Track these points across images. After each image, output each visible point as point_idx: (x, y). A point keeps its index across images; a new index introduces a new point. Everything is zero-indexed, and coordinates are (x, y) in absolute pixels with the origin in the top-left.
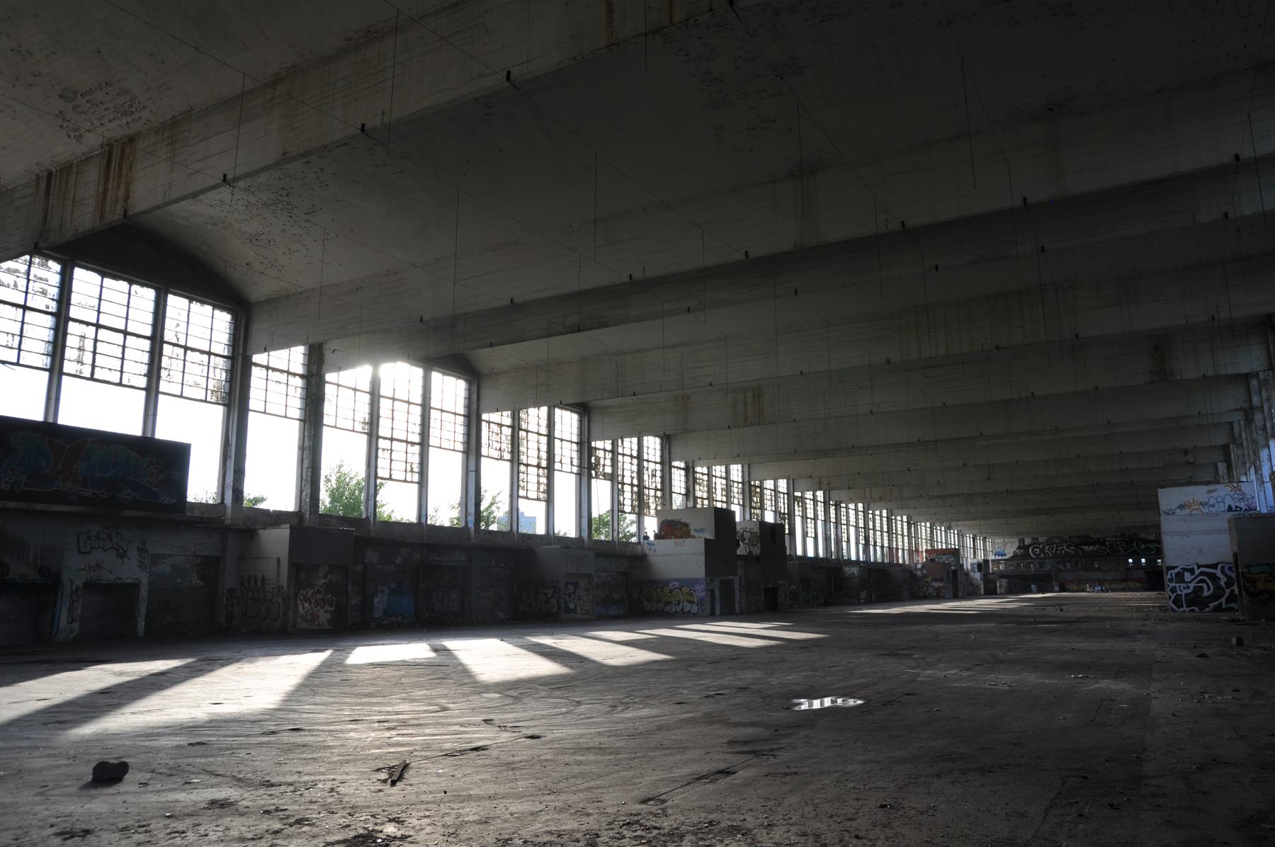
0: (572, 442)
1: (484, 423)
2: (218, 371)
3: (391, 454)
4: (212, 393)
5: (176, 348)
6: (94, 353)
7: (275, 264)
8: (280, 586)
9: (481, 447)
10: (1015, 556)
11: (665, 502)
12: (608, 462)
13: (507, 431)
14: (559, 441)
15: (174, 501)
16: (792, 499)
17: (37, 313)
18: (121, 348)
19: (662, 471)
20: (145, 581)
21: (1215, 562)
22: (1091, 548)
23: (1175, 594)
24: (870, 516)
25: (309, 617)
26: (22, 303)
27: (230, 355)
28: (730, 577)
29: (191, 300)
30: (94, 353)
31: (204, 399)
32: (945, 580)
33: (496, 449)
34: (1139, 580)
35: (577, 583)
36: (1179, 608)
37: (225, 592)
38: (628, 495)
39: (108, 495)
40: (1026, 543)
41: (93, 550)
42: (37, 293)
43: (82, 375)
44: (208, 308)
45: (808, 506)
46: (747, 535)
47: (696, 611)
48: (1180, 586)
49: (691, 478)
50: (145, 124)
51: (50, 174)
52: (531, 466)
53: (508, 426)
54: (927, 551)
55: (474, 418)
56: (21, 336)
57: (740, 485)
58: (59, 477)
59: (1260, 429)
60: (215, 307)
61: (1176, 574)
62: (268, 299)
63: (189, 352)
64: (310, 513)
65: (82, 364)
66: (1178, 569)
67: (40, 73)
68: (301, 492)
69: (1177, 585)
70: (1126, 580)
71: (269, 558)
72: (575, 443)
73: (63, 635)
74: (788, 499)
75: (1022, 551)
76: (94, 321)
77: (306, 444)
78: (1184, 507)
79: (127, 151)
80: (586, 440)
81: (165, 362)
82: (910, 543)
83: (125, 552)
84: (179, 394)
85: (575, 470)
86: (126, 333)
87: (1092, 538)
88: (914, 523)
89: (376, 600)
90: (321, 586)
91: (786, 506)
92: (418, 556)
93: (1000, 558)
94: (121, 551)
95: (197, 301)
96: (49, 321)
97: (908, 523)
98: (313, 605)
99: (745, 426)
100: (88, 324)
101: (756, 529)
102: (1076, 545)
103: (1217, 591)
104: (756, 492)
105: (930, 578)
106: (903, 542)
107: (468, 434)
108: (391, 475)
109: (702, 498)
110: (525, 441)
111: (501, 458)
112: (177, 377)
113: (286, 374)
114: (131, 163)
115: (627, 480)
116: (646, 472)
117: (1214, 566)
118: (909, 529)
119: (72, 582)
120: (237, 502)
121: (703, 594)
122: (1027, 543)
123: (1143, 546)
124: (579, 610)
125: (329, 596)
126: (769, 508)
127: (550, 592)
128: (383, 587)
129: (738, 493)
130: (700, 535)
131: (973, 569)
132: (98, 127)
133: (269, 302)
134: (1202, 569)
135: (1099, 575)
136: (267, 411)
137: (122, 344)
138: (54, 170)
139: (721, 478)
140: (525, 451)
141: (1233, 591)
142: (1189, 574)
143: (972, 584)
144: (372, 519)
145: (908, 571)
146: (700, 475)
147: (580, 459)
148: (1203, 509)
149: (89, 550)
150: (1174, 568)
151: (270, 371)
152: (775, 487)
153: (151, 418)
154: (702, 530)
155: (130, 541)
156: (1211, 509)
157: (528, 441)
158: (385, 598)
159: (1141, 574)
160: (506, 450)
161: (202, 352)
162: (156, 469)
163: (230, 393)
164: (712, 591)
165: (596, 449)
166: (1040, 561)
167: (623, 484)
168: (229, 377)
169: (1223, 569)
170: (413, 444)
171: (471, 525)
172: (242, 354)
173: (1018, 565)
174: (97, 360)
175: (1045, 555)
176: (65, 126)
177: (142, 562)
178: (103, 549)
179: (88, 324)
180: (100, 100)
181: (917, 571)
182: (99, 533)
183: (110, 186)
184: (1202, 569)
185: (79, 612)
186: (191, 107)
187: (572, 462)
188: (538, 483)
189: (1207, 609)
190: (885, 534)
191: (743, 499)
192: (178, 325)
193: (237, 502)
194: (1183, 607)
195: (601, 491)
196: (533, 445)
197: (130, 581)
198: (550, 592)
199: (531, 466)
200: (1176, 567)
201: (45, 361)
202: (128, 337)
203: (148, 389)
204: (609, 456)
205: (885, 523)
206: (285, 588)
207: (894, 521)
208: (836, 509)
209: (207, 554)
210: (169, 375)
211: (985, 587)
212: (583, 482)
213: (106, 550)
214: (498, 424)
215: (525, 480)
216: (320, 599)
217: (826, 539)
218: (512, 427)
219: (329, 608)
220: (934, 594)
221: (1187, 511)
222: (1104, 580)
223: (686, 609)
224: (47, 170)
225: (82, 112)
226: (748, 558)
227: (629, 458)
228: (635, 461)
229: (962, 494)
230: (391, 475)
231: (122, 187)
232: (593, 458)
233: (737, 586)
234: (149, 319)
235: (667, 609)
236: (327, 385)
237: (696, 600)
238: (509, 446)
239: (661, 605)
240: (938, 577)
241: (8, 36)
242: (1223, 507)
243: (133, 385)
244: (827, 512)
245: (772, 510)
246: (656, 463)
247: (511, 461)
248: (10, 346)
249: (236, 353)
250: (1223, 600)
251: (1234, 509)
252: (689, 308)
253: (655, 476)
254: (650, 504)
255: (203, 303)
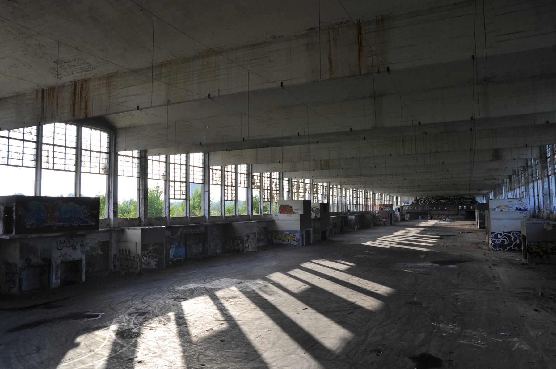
0: (244, 174)
1: (210, 170)
2: (104, 160)
3: (174, 188)
4: (102, 170)
5: (86, 151)
6: (53, 157)
7: (130, 114)
8: (137, 254)
9: (210, 180)
10: (413, 204)
11: (281, 196)
12: (259, 181)
13: (219, 172)
14: (240, 174)
15: (94, 224)
16: (329, 188)
17: (29, 142)
18: (64, 154)
19: (279, 182)
20: (84, 258)
21: (510, 231)
22: (444, 201)
23: (494, 243)
24: (358, 192)
25: (146, 263)
26: (22, 138)
27: (108, 152)
28: (309, 229)
29: (91, 129)
30: (53, 157)
31: (99, 173)
32: (387, 218)
33: (215, 181)
34: (463, 215)
35: (249, 236)
36: (495, 249)
37: (113, 256)
38: (266, 194)
39: (68, 225)
40: (418, 199)
41: (63, 248)
42: (28, 133)
43: (49, 168)
44: (99, 131)
45: (335, 191)
46: (314, 209)
47: (296, 244)
48: (496, 240)
49: (290, 184)
50: (94, 75)
51: (43, 91)
52: (229, 186)
53: (220, 170)
54: (379, 205)
55: (207, 168)
56: (23, 153)
57: (309, 185)
58: (49, 220)
59: (530, 175)
60: (101, 131)
61: (495, 235)
62: (125, 127)
63: (92, 152)
64: (144, 218)
65: (49, 163)
66: (496, 233)
67: (47, 53)
68: (140, 209)
69: (495, 240)
70: (458, 215)
71: (132, 242)
72: (246, 174)
73: (54, 285)
74: (327, 189)
75: (416, 202)
76: (52, 143)
77: (141, 188)
78: (499, 207)
79: (84, 86)
80: (250, 173)
81: (83, 158)
82: (373, 202)
83: (75, 247)
84: (89, 172)
85: (246, 186)
86: (65, 147)
87: (445, 197)
88: (374, 193)
89: (171, 251)
90: (151, 250)
91: (326, 191)
92: (186, 231)
93: (407, 204)
94: (74, 247)
95: (94, 129)
96: (34, 145)
97: (372, 193)
98: (148, 258)
99: (321, 170)
100: (50, 145)
101: (318, 207)
102: (438, 200)
103: (510, 242)
104: (315, 187)
105: (381, 217)
106: (370, 202)
107: (204, 176)
108: (174, 197)
109: (294, 192)
110: (227, 176)
111: (217, 185)
112: (87, 164)
113: (131, 158)
114: (87, 92)
115: (266, 188)
116: (273, 183)
117: (510, 233)
118: (373, 196)
119: (56, 263)
120: (115, 217)
121: (299, 237)
122: (418, 198)
123: (465, 201)
124: (250, 247)
125: (155, 254)
126: (320, 193)
127: (239, 241)
128: (173, 245)
129: (308, 188)
130: (297, 211)
131: (396, 210)
132: (70, 74)
133: (125, 129)
134: (505, 234)
135: (447, 213)
136: (125, 175)
137: (64, 152)
138: (45, 89)
139: (302, 182)
140: (227, 180)
141: (516, 243)
142: (500, 235)
143: (396, 217)
144: (168, 217)
145: (373, 215)
146: (294, 182)
147: (248, 181)
148: (506, 209)
149: (61, 248)
150: (494, 233)
151: (125, 157)
152: (322, 186)
153: (78, 184)
154: (298, 209)
155: (77, 242)
156: (510, 209)
157: (227, 175)
158: (174, 249)
159: (464, 212)
160: (219, 180)
161: (97, 152)
162: (87, 211)
163: (109, 169)
164: (302, 236)
165: (254, 176)
166: (423, 206)
167: (264, 190)
168: (108, 162)
169: (513, 233)
170: (183, 182)
171: (206, 215)
172: (114, 152)
173: (414, 207)
174: (55, 161)
175: (425, 203)
176: (54, 73)
177: (82, 251)
178: (67, 247)
179: (50, 145)
180: (74, 65)
181: (376, 214)
182: (64, 240)
183: (77, 101)
184: (505, 234)
185: (59, 275)
186: (118, 71)
187: (244, 182)
188: (232, 193)
189: (506, 250)
190: (364, 199)
191: (310, 191)
192: (87, 141)
193: (115, 217)
194: (496, 248)
195: (256, 193)
196: (229, 177)
197: (78, 259)
198: (239, 241)
199: (229, 186)
200: (495, 232)
201: (33, 164)
202: (67, 149)
203: (76, 172)
204: (259, 178)
205: (363, 194)
206: (140, 255)
207: (367, 193)
208: (345, 191)
209: (104, 240)
210: (84, 164)
211: (401, 217)
212: (249, 190)
213: (68, 247)
214: (216, 170)
215: (227, 193)
216: (151, 256)
217: (341, 204)
218: (221, 170)
219: (155, 260)
220: (383, 224)
221: (500, 209)
222: (449, 215)
223: (292, 243)
224: (42, 89)
225: (64, 69)
226: (317, 219)
227: (267, 178)
228: (269, 179)
229: (399, 186)
230: (174, 197)
231: (83, 103)
232: (253, 180)
233: (311, 232)
234: (74, 139)
235: (284, 243)
236: (148, 161)
237: (296, 240)
238: (220, 179)
239: (281, 241)
240: (385, 217)
241: (35, 40)
242: (515, 208)
243: (70, 170)
244: (342, 192)
245: (321, 194)
246: (277, 179)
247: (221, 185)
248: (19, 158)
249: (111, 151)
250: (512, 246)
251: (519, 209)
252: (317, 142)
253: (276, 185)
254: (275, 197)
255: (96, 129)
